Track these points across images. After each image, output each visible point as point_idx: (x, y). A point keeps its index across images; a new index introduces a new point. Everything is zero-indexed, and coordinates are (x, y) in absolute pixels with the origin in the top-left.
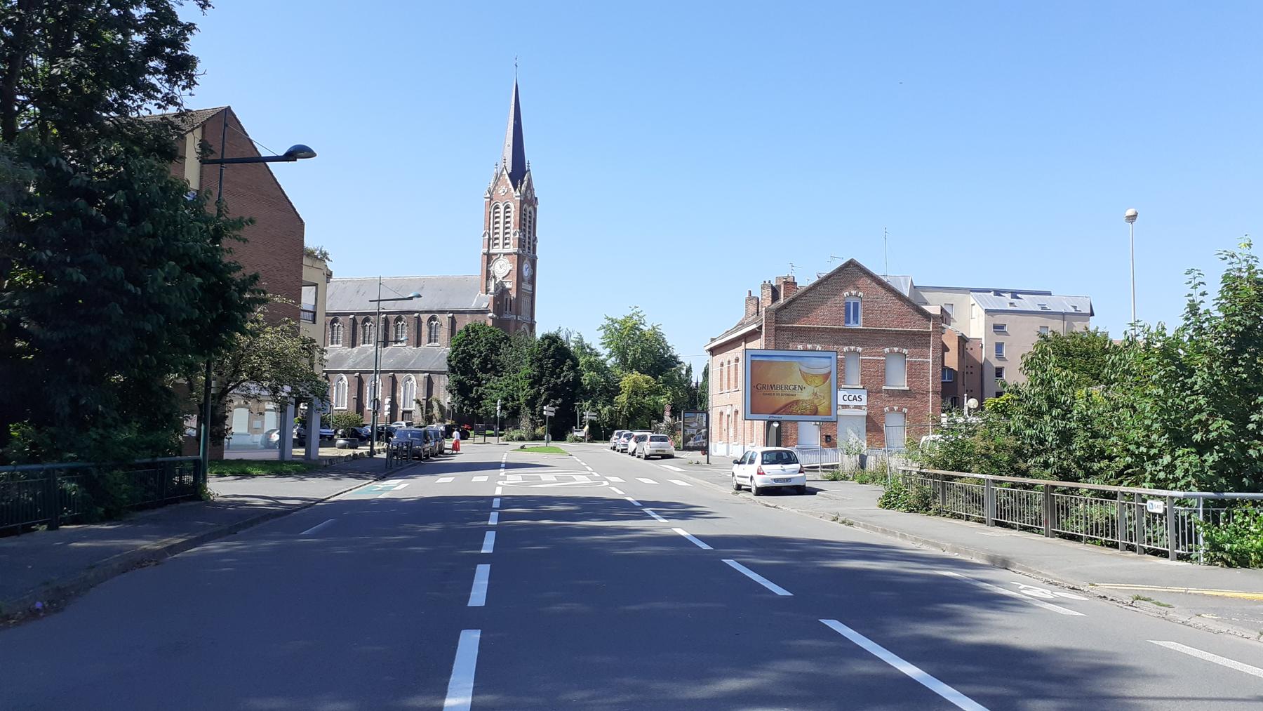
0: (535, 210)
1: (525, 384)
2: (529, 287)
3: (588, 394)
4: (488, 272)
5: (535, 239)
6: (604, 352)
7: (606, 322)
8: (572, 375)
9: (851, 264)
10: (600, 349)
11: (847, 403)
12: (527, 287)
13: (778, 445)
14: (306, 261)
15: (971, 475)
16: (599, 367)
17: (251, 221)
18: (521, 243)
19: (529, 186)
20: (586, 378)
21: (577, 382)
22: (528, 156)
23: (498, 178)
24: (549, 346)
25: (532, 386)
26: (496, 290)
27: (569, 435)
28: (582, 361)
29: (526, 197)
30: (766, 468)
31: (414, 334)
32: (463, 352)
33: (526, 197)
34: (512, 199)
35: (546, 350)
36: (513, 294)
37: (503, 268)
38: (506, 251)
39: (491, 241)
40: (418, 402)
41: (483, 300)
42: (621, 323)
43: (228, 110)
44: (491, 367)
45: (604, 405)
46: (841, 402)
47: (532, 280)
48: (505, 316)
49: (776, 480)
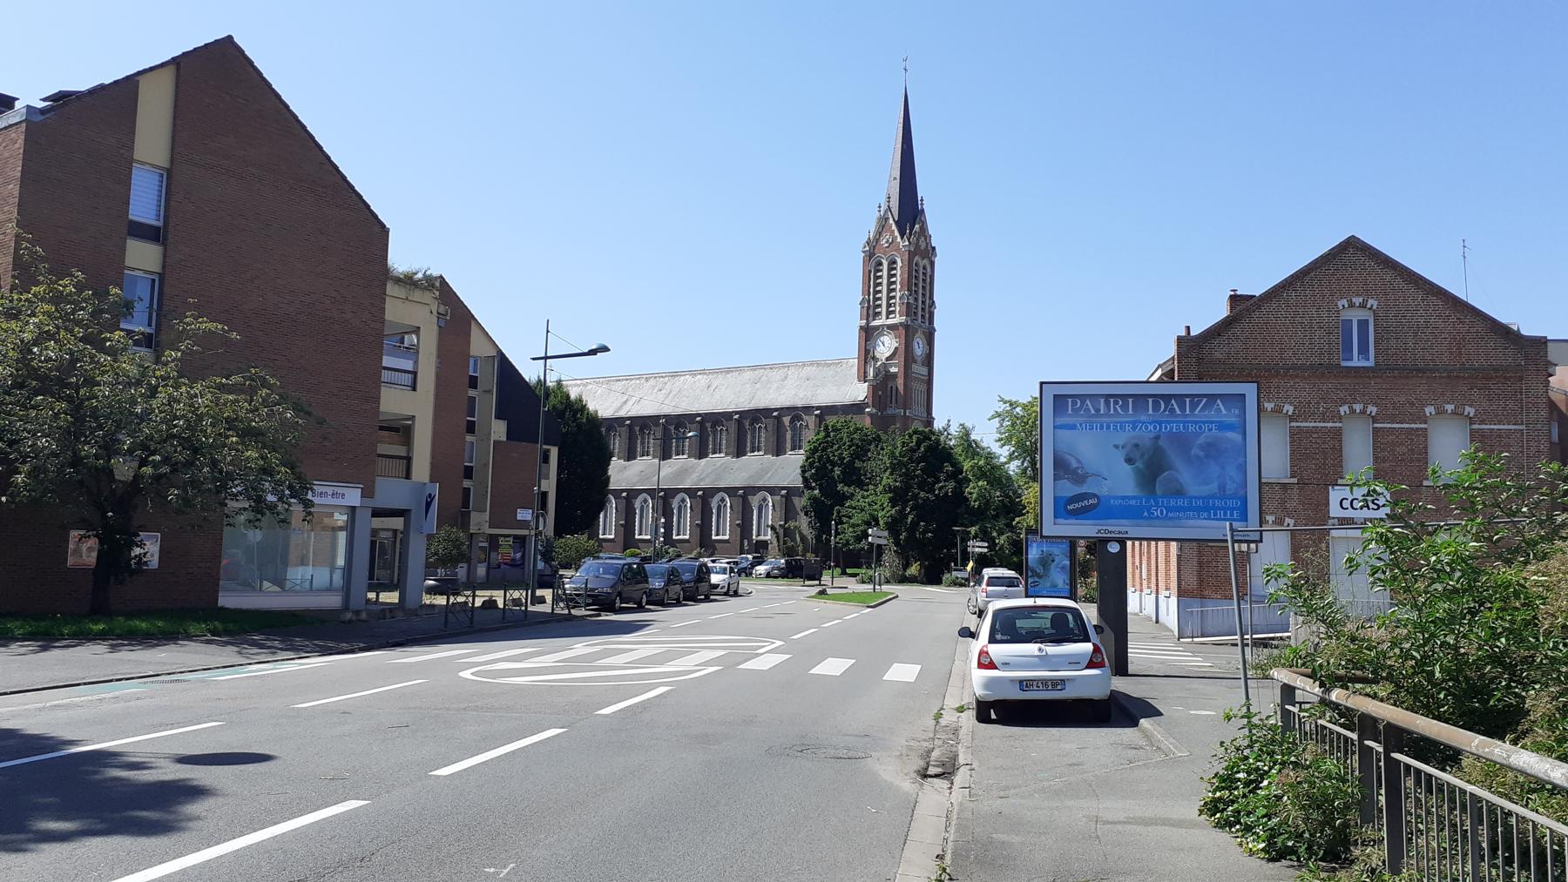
0: (932, 264)
1: (884, 499)
2: (924, 371)
3: (978, 515)
4: (867, 352)
5: (933, 304)
6: (1002, 452)
7: (1001, 407)
8: (951, 485)
9: (1352, 248)
10: (995, 448)
11: (1349, 513)
12: (921, 370)
13: (1231, 598)
14: (391, 289)
15: (1499, 750)
16: (992, 473)
17: (1116, 447)
18: (910, 310)
19: (924, 229)
20: (973, 490)
21: (959, 497)
22: (922, 191)
23: (883, 221)
24: (918, 444)
25: (893, 502)
26: (876, 375)
27: (946, 577)
28: (967, 465)
29: (917, 246)
30: (999, 651)
31: (773, 439)
32: (820, 458)
33: (917, 246)
34: (898, 249)
35: (913, 450)
36: (900, 382)
37: (886, 346)
38: (889, 322)
39: (870, 310)
40: (773, 528)
41: (858, 392)
42: (1024, 407)
43: (230, 38)
44: (855, 477)
45: (1001, 533)
46: (1335, 511)
47: (929, 360)
48: (890, 411)
49: (1024, 684)
